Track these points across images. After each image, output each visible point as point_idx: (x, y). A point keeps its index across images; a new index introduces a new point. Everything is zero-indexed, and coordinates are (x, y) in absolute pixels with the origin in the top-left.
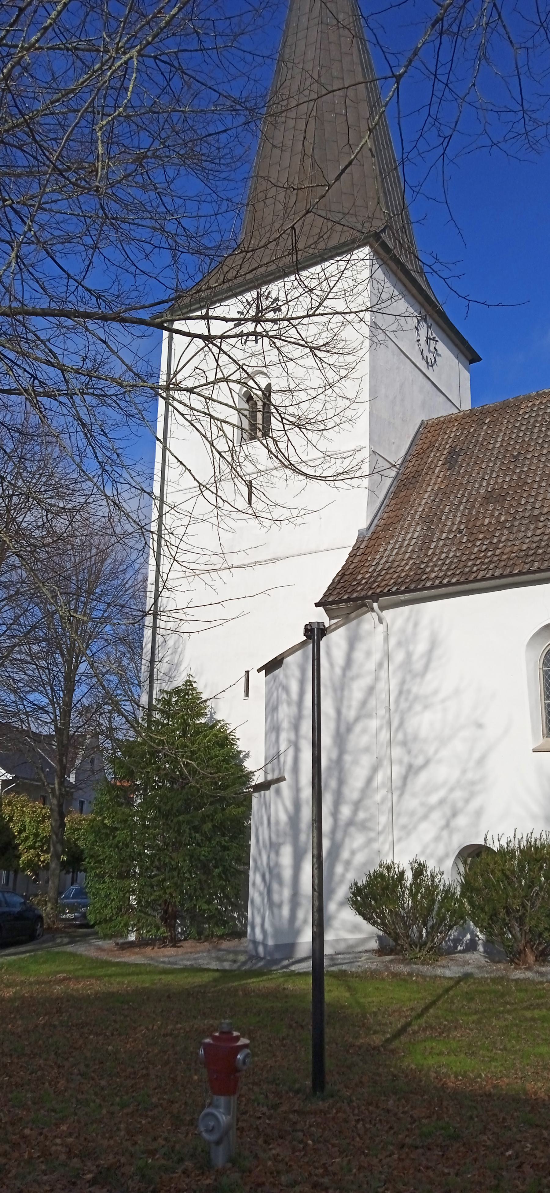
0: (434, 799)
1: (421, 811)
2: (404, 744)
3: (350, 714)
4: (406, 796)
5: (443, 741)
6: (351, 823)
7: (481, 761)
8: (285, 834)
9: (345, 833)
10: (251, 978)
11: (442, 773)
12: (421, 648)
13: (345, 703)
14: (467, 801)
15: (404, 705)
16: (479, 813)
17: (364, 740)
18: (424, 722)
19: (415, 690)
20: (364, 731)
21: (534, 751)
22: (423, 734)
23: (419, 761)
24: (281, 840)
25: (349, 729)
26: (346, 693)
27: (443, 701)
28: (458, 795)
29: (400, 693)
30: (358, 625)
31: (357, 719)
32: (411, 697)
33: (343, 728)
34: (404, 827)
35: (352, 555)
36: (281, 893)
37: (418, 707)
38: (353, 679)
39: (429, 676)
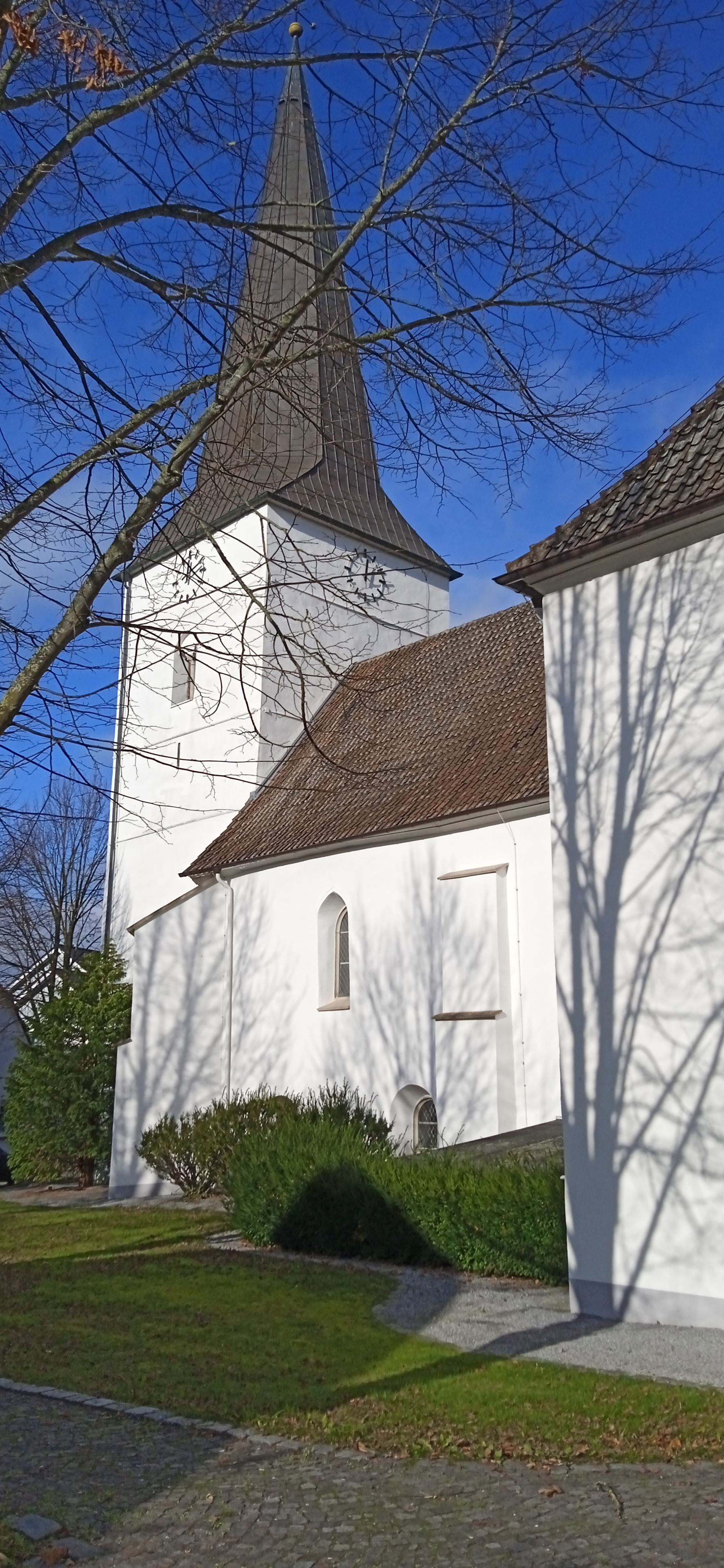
0: (257, 1055)
1: (249, 1066)
2: (241, 1004)
3: (201, 978)
4: (241, 1052)
5: (265, 1002)
6: (196, 1078)
7: (288, 1020)
8: (131, 1090)
9: (190, 1088)
10: (248, 1252)
11: (263, 1031)
12: (254, 914)
13: (196, 968)
14: (278, 1056)
15: (242, 968)
16: (284, 1067)
17: (214, 1002)
18: (255, 984)
19: (249, 954)
20: (214, 993)
21: (320, 1010)
22: (253, 995)
23: (249, 1020)
24: (126, 1096)
25: (199, 992)
26: (197, 959)
27: (267, 964)
28: (273, 1051)
29: (241, 957)
30: (212, 893)
31: (208, 982)
32: (247, 960)
33: (192, 990)
34: (238, 1080)
35: (235, 820)
36: (124, 1143)
37: (251, 970)
38: (203, 945)
39: (259, 941)
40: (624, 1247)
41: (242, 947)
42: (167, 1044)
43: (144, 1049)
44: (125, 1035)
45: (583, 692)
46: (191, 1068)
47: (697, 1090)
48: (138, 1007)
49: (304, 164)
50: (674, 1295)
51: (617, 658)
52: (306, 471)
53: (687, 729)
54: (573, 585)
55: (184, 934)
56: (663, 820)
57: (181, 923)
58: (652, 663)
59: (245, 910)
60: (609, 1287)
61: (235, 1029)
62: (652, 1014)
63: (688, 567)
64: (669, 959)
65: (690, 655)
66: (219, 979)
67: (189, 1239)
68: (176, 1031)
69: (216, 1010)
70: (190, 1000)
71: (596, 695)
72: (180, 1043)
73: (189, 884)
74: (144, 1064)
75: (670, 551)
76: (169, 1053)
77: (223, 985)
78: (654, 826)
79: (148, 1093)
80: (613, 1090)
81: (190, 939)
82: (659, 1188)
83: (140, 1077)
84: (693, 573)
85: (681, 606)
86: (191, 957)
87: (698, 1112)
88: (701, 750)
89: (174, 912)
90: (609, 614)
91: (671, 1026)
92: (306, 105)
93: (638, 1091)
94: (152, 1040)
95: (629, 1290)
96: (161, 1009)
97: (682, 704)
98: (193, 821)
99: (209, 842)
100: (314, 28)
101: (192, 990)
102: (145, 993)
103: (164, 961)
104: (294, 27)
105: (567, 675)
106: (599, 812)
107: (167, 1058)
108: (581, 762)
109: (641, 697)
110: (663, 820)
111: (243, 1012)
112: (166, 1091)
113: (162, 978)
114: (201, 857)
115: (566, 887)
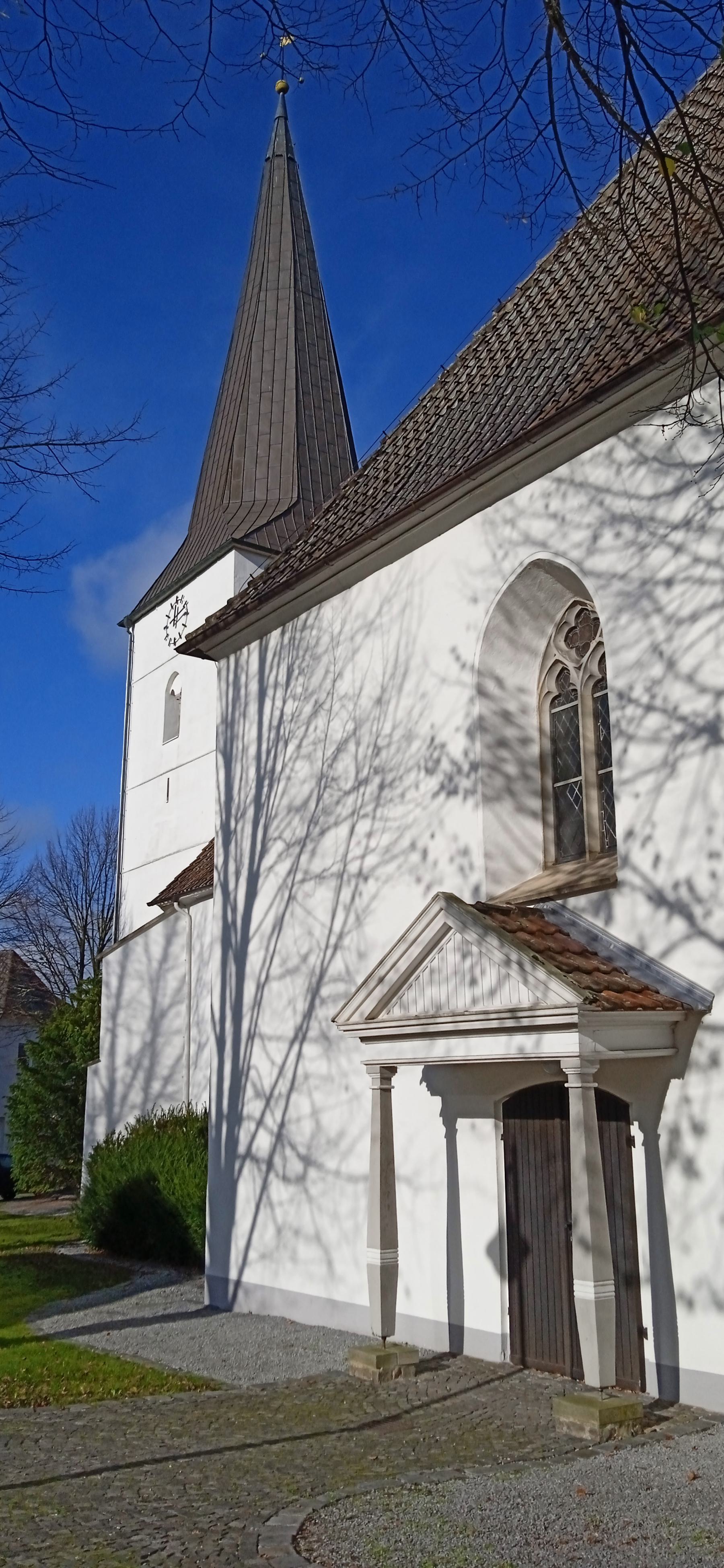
3: (165, 1001)
4: (198, 1069)
6: (160, 1095)
13: (160, 992)
15: (199, 990)
19: (204, 977)
20: (178, 1015)
24: (97, 1112)
25: (163, 1014)
26: (162, 984)
29: (197, 980)
31: (171, 1006)
33: (157, 1013)
38: (168, 970)
40: (236, 1245)
41: (199, 971)
42: (134, 1063)
43: (112, 1069)
44: (94, 1057)
45: (237, 748)
46: (156, 1086)
47: (282, 1103)
48: (107, 1029)
49: (287, 216)
50: (262, 1287)
51: (256, 717)
52: (279, 513)
53: (293, 781)
54: (235, 652)
55: (149, 960)
56: (276, 863)
57: (147, 950)
58: (275, 723)
59: (200, 936)
60: (226, 1280)
61: (193, 1048)
62: (262, 1037)
63: (298, 635)
64: (274, 986)
65: (296, 714)
66: (180, 1002)
67: (25, 1244)
68: (142, 1051)
69: (178, 1032)
70: (156, 1022)
71: (245, 749)
72: (146, 1063)
73: (157, 911)
74: (112, 1083)
75: (289, 622)
76: (135, 1072)
77: (183, 1008)
78: (271, 868)
79: (116, 1110)
80: (237, 1106)
81: (155, 965)
82: (258, 1191)
83: (109, 1094)
84: (301, 639)
85: (293, 671)
86: (155, 981)
87: (282, 1125)
88: (298, 802)
89: (139, 939)
90: (254, 677)
91: (272, 1046)
92: (291, 160)
93: (252, 1107)
94: (120, 1060)
95: (238, 1283)
96: (129, 1031)
97: (290, 759)
98: (178, 852)
99: (179, 872)
100: (302, 82)
101: (157, 1013)
102: (114, 1016)
103: (132, 986)
104: (280, 84)
105: (229, 734)
106: (241, 855)
107: (134, 1077)
108: (233, 811)
109: (268, 752)
110: (276, 863)
111: (199, 1032)
112: (133, 1107)
113: (130, 1003)
114: (169, 886)
115: (220, 924)
